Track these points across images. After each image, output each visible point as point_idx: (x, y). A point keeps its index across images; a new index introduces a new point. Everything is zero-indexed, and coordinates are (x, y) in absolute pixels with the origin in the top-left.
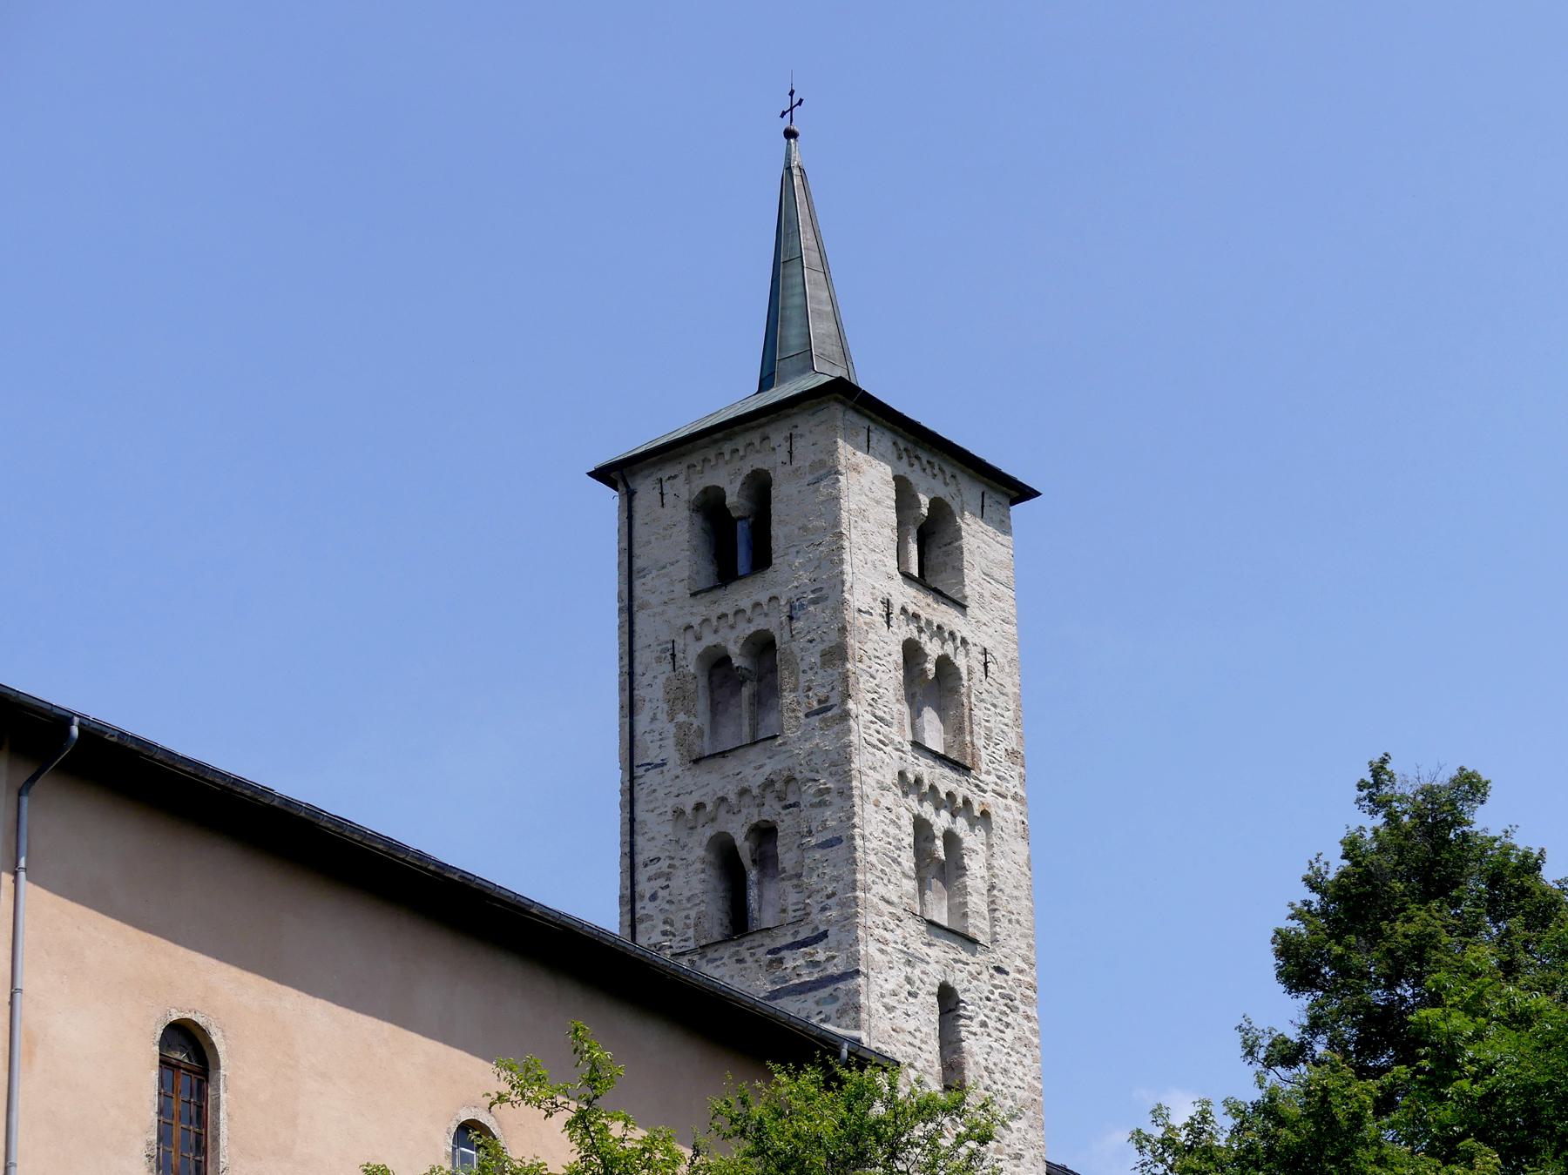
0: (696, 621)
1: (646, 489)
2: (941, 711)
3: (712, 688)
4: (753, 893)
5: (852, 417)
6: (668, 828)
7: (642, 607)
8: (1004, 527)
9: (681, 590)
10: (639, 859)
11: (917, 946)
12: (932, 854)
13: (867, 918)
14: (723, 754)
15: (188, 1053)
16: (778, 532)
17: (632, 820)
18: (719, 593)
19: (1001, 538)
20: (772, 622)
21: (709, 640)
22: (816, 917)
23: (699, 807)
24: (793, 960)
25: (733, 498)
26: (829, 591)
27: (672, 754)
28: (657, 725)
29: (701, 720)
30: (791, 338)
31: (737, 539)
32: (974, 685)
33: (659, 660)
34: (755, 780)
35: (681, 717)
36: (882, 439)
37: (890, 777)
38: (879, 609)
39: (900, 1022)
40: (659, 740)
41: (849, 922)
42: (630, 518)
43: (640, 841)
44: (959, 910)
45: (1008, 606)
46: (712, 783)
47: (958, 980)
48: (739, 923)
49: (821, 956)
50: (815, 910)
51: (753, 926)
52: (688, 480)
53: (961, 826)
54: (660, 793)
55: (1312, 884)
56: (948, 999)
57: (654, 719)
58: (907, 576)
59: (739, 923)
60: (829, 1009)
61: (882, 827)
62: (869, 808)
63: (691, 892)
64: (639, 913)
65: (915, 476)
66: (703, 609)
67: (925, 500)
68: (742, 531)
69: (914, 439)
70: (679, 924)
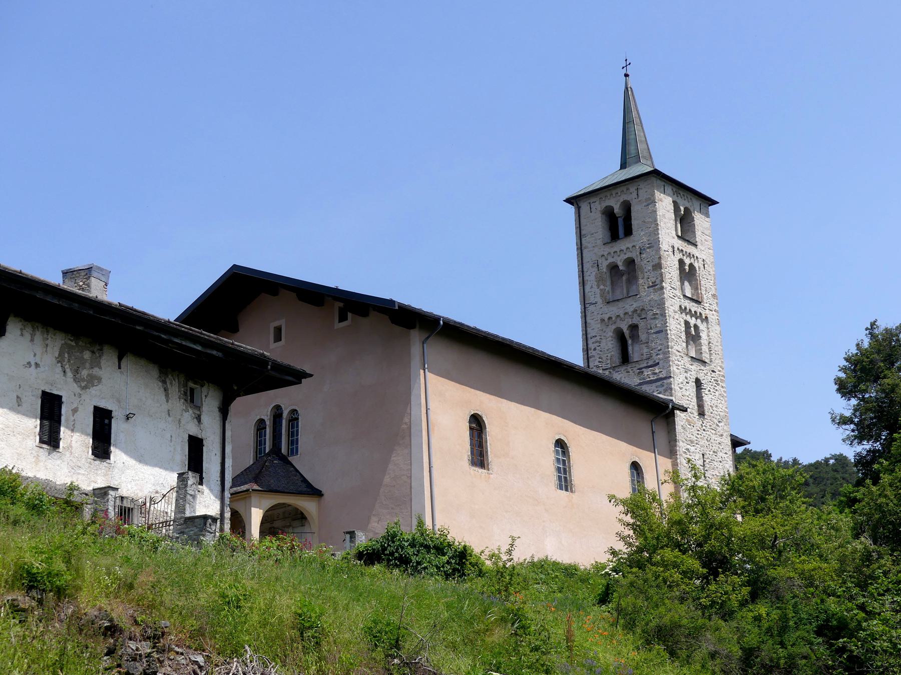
0: (605, 254)
1: (585, 207)
2: (690, 282)
3: (611, 276)
4: (630, 348)
5: (659, 182)
6: (599, 326)
7: (585, 248)
8: (707, 215)
9: (599, 242)
10: (589, 336)
11: (688, 365)
12: (690, 333)
13: (673, 358)
14: (618, 300)
15: (477, 424)
16: (634, 223)
17: (586, 322)
18: (614, 244)
19: (707, 219)
20: (634, 255)
21: (610, 260)
22: (654, 357)
23: (610, 318)
24: (647, 372)
25: (617, 210)
26: (654, 244)
27: (599, 300)
28: (593, 290)
29: (608, 288)
30: (632, 150)
31: (619, 225)
32: (701, 273)
33: (592, 267)
34: (630, 310)
35: (602, 287)
36: (669, 189)
37: (677, 308)
38: (671, 250)
39: (684, 393)
40: (594, 294)
41: (667, 359)
42: (579, 216)
43: (589, 330)
44: (699, 351)
45: (710, 244)
46: (614, 310)
47: (701, 376)
48: (625, 358)
49: (657, 371)
50: (654, 355)
51: (631, 360)
52: (600, 203)
53: (699, 322)
54: (595, 313)
55: (847, 360)
56: (698, 382)
57: (592, 287)
58: (678, 236)
59: (625, 358)
60: (661, 389)
61: (675, 325)
62: (671, 319)
63: (609, 347)
64: (590, 355)
65: (679, 200)
66: (607, 250)
67: (682, 208)
68: (620, 222)
69: (679, 187)
70: (604, 359)
